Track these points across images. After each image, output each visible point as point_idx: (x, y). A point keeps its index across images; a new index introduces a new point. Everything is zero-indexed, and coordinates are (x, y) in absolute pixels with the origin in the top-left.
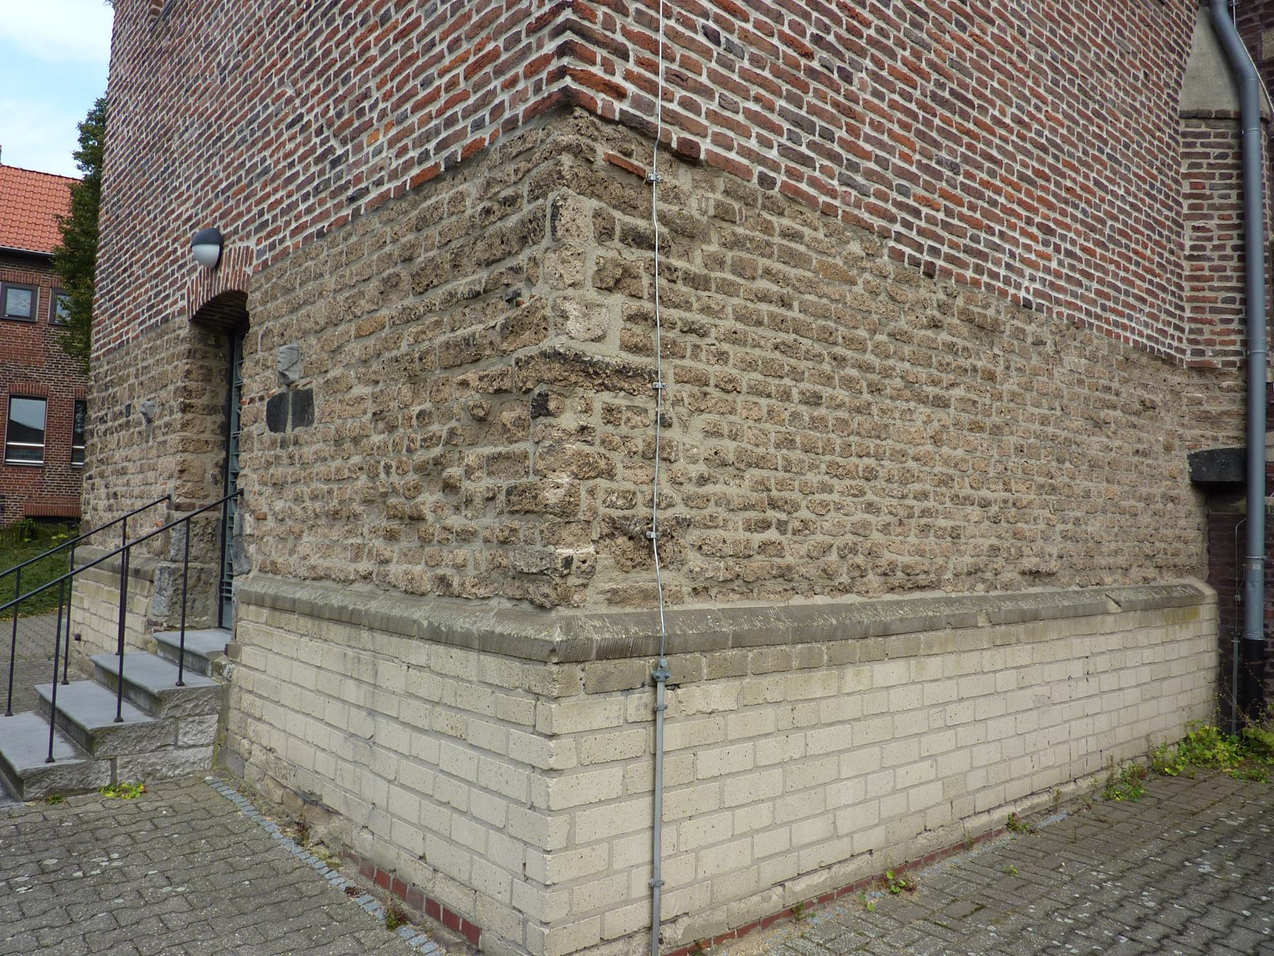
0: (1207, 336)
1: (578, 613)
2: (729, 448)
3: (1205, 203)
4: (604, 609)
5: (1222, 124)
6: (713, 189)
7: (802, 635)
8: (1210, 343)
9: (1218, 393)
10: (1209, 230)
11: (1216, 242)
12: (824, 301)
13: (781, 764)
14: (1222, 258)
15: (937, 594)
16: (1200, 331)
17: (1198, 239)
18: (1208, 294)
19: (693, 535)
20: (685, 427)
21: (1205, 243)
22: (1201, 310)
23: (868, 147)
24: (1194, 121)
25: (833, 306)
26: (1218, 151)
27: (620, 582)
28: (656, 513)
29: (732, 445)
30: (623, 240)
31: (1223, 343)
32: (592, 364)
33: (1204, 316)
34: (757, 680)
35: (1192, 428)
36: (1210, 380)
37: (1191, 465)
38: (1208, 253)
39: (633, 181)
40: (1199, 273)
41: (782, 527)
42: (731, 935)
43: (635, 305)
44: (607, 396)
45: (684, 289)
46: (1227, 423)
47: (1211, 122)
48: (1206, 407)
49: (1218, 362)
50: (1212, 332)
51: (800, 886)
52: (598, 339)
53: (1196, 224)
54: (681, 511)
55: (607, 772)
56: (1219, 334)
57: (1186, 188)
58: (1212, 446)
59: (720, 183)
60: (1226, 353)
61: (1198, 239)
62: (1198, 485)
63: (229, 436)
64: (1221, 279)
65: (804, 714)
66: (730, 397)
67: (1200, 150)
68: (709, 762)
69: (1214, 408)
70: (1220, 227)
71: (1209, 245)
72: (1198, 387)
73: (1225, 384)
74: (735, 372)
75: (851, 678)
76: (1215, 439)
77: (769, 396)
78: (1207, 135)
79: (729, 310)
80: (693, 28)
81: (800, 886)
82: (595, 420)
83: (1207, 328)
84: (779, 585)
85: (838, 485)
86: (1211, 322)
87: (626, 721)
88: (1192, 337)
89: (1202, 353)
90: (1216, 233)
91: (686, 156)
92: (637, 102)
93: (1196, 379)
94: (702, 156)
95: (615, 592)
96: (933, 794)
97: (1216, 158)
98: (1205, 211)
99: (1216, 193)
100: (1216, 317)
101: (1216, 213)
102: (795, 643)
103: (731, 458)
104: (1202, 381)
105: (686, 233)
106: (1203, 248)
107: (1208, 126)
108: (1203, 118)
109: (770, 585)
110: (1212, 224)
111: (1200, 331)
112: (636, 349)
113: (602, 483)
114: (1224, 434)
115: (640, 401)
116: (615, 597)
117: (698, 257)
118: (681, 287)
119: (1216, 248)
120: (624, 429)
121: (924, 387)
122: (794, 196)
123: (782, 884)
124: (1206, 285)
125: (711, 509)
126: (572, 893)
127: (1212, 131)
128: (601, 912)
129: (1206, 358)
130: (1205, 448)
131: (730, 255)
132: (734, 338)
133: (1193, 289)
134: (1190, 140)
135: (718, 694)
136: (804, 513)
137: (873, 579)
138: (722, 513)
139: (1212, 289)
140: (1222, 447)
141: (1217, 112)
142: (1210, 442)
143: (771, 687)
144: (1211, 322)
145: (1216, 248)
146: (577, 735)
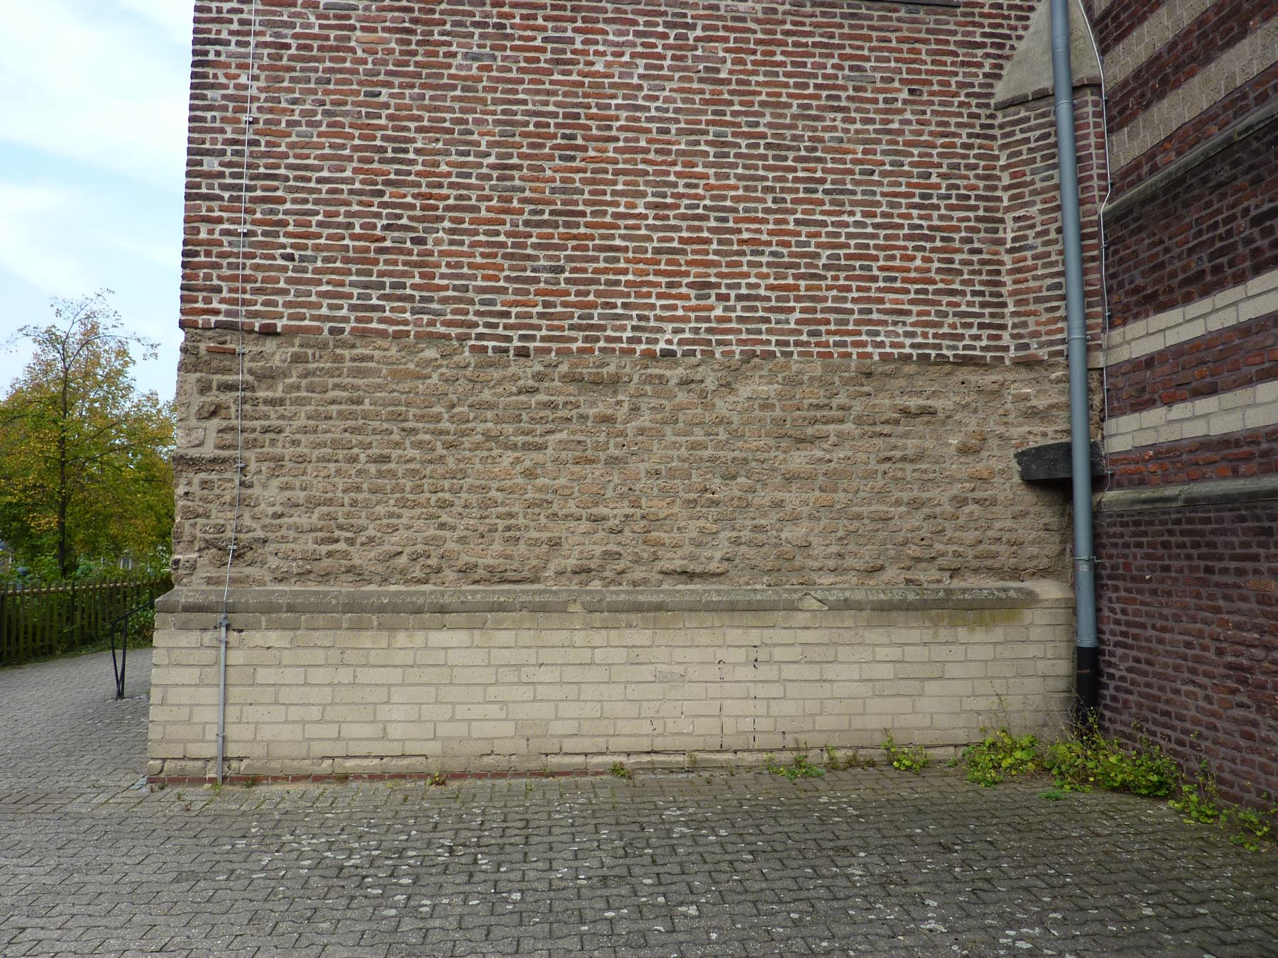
0: (1032, 328)
1: (185, 589)
2: (300, 496)
3: (1026, 190)
4: (204, 587)
5: (1043, 103)
6: (293, 346)
7: (349, 608)
8: (1035, 334)
9: (1047, 386)
10: (1032, 218)
11: (1039, 229)
12: (395, 394)
13: (330, 684)
14: (1045, 244)
15: (536, 587)
16: (1025, 324)
17: (1020, 229)
18: (1032, 284)
19: (271, 547)
20: (264, 486)
21: (1027, 232)
22: (1025, 302)
23: (445, 282)
24: (1012, 109)
25: (403, 397)
26: (1038, 133)
27: (213, 572)
28: (242, 536)
29: (302, 494)
30: (219, 389)
31: (1049, 333)
32: (191, 459)
33: (1028, 308)
34: (309, 632)
35: (1021, 425)
36: (1040, 372)
37: (1019, 464)
38: (1030, 242)
39: (229, 356)
40: (1021, 264)
41: (350, 542)
42: (287, 779)
43: (225, 423)
44: (203, 475)
45: (265, 408)
46: (1057, 417)
47: (1029, 105)
48: (1034, 402)
49: (1043, 353)
50: (1038, 324)
51: (350, 763)
52: (200, 445)
53: (1017, 214)
54: (260, 534)
55: (189, 670)
56: (1044, 324)
57: (1006, 180)
58: (1042, 442)
59: (297, 341)
60: (1052, 343)
61: (1020, 229)
62: (1031, 482)
63: (1230, 461)
64: (1045, 266)
65: (350, 657)
66: (302, 466)
67: (1019, 136)
68: (264, 675)
69: (1041, 403)
70: (1042, 212)
71: (1031, 233)
72: (1028, 382)
73: (1053, 376)
74: (306, 451)
75: (401, 638)
76: (1045, 435)
77: (336, 461)
78: (1027, 119)
79: (303, 414)
80: (274, 258)
81: (350, 763)
82: (195, 488)
83: (1031, 320)
84: (350, 577)
85: (406, 513)
86: (1035, 313)
87: (202, 645)
88: (1015, 331)
89: (1026, 347)
90: (1039, 218)
91: (269, 332)
92: (228, 313)
93: (1024, 374)
94: (279, 330)
95: (210, 578)
96: (507, 729)
97: (1036, 141)
98: (1027, 199)
99: (1037, 177)
100: (1041, 307)
101: (1038, 198)
102: (344, 612)
103: (301, 501)
104: (1032, 375)
105: (268, 376)
106: (1025, 238)
107: (1027, 110)
108: (1021, 103)
109: (343, 577)
110: (1033, 211)
111: (1025, 324)
112: (223, 447)
113: (200, 521)
114: (1055, 428)
115: (227, 475)
116: (209, 581)
117: (280, 388)
118: (262, 408)
119: (1038, 235)
120: (216, 491)
121: (512, 438)
122: (363, 334)
123: (333, 758)
124: (1029, 275)
125: (283, 532)
126: (165, 728)
127: (1032, 114)
128: (185, 742)
129: (1032, 351)
130: (1032, 445)
131: (304, 382)
132: (304, 430)
133: (1015, 282)
134: (1008, 129)
135: (275, 638)
136: (371, 532)
137: (449, 575)
138: (292, 534)
139: (1035, 278)
140: (1051, 442)
141: (1033, 93)
142: (1039, 438)
143: (322, 638)
144: (1035, 313)
145: (1038, 235)
146: (168, 648)
